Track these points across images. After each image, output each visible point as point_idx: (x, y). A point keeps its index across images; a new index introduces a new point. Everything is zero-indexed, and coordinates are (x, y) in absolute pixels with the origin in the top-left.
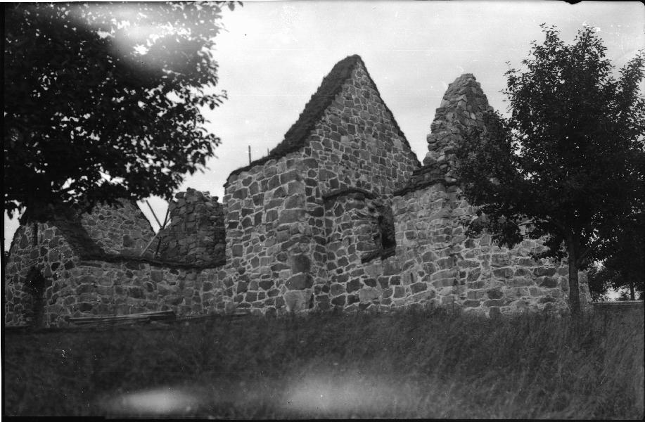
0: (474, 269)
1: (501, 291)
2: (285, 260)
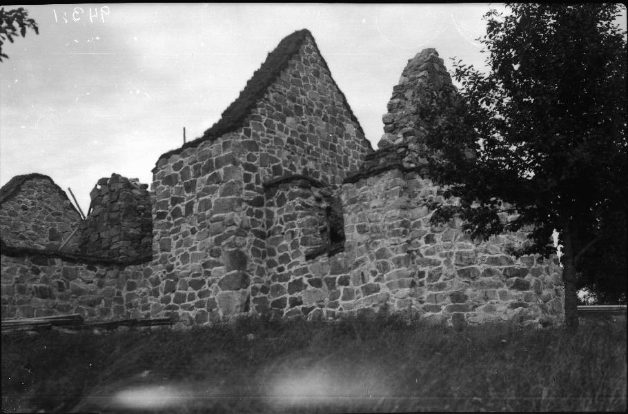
0: (434, 268)
1: (465, 294)
2: (218, 256)
